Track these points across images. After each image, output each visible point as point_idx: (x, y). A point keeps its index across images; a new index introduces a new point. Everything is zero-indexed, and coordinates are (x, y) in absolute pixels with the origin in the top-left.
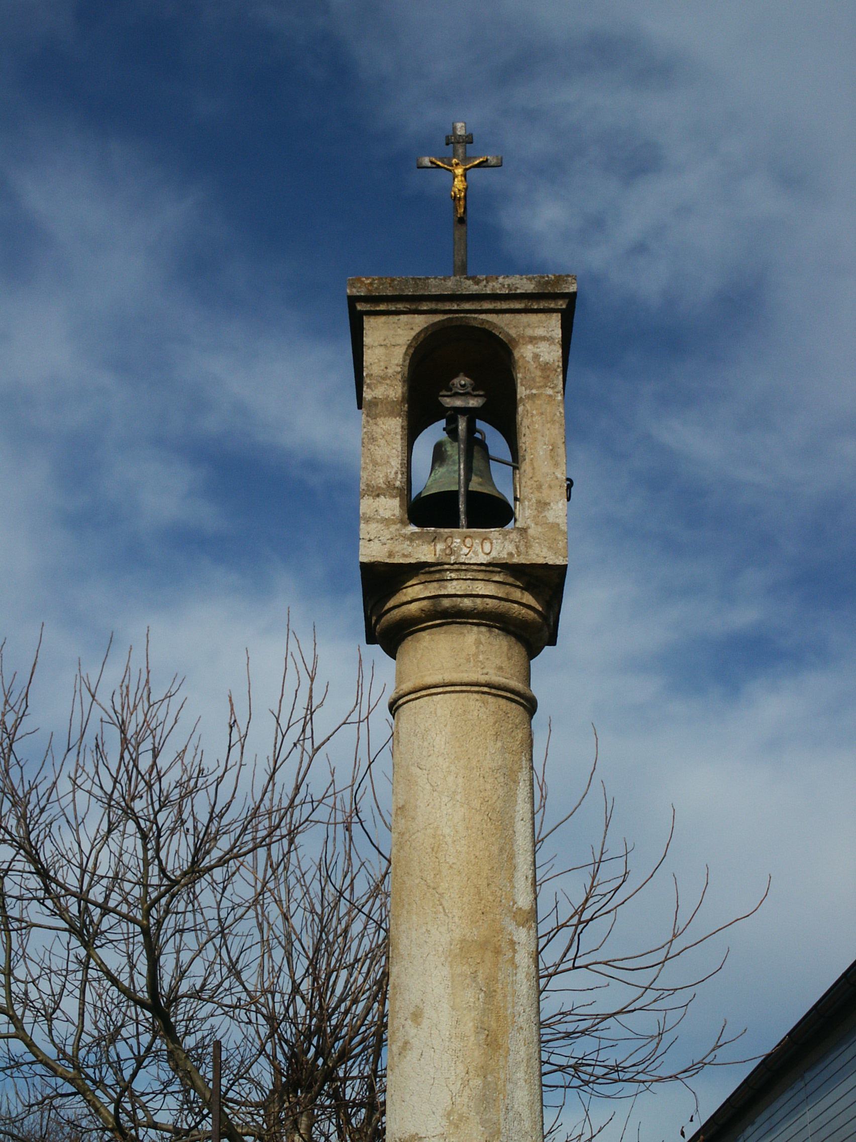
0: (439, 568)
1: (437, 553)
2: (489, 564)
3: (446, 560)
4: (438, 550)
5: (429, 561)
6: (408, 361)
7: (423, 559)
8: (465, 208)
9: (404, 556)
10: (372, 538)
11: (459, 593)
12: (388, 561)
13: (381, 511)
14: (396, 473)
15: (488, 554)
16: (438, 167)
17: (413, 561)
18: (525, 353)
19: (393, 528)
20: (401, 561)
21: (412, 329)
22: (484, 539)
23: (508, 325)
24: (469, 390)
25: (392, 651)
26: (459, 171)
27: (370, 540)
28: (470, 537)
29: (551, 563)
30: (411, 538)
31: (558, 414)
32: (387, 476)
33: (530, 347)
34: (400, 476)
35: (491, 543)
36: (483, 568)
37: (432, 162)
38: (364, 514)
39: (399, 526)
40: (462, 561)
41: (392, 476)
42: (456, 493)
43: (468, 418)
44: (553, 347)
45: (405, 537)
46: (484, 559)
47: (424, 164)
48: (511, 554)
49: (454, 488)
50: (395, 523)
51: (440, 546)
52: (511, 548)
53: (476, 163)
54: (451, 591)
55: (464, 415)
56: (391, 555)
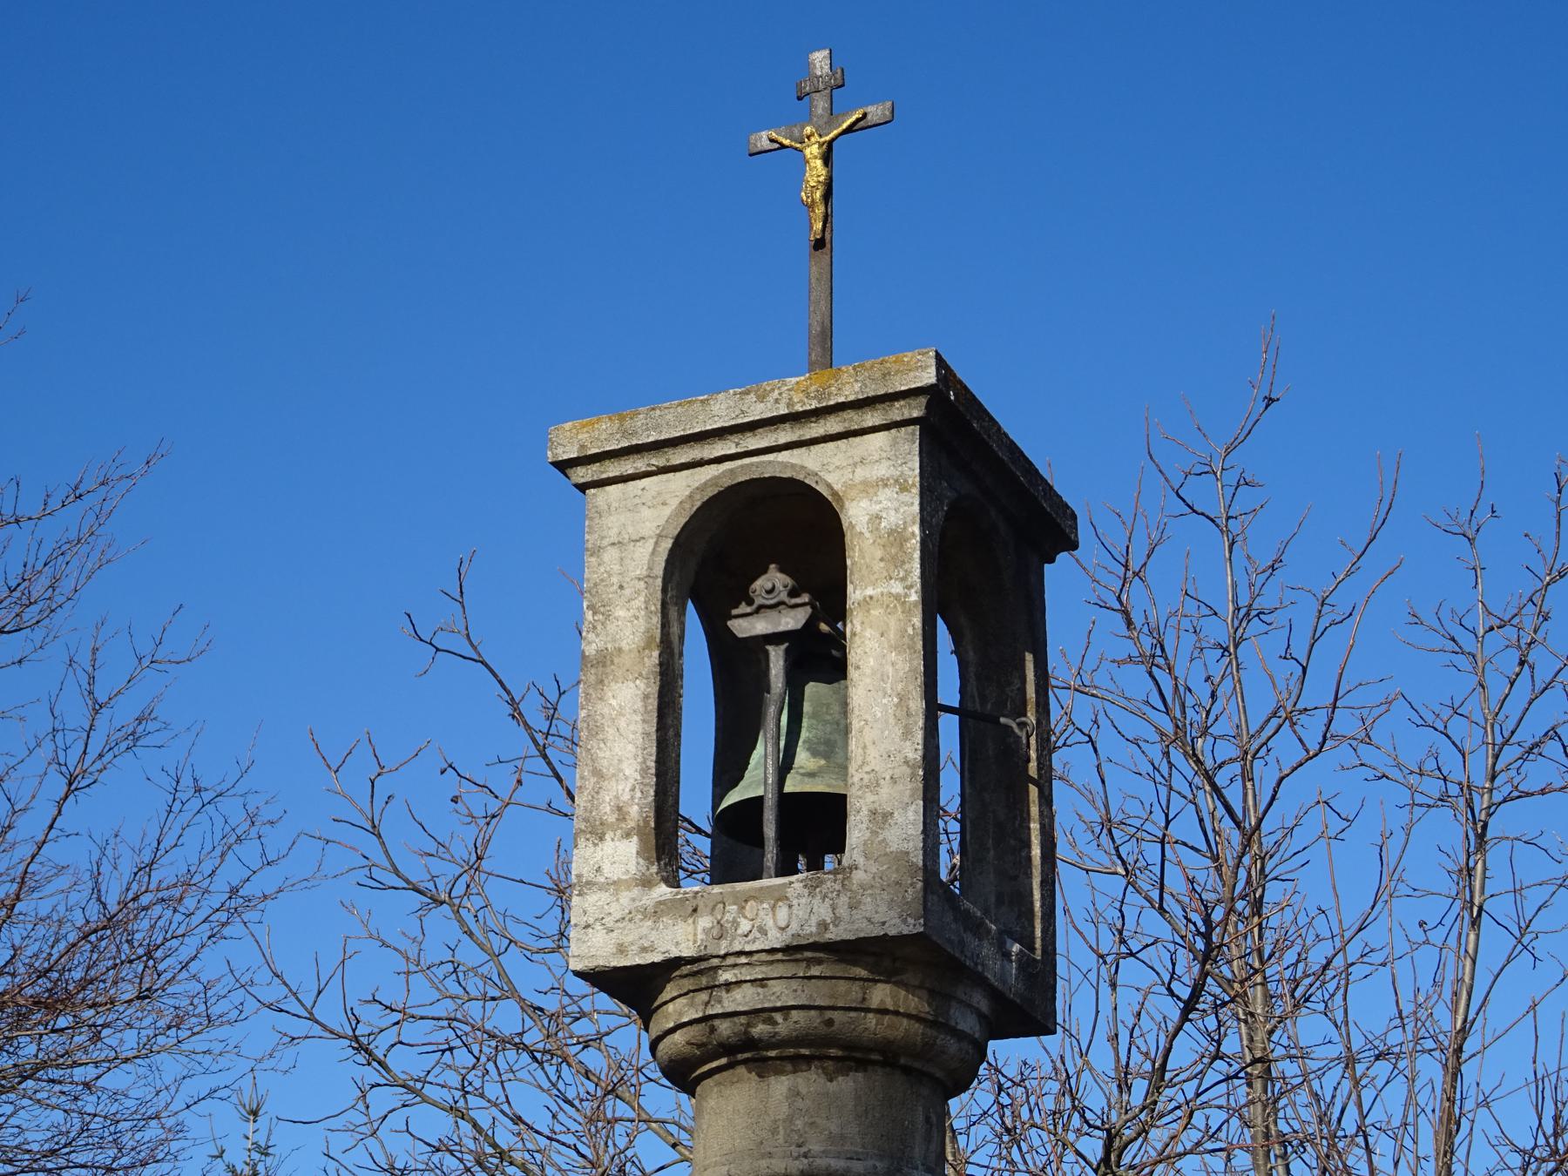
0: (703, 965)
1: (700, 937)
2: (787, 949)
3: (710, 951)
4: (700, 930)
5: (684, 955)
6: (825, 493)
7: (675, 953)
8: (826, 219)
9: (644, 950)
10: (591, 921)
11: (741, 1008)
12: (615, 963)
13: (606, 868)
14: (633, 790)
15: (783, 929)
16: (783, 146)
17: (657, 958)
18: (856, 515)
19: (625, 897)
20: (638, 961)
21: (664, 504)
22: (779, 900)
23: (823, 466)
24: (784, 596)
25: (692, 1094)
26: (813, 150)
27: (587, 926)
28: (754, 898)
29: (893, 932)
30: (657, 912)
31: (910, 631)
32: (617, 797)
33: (864, 503)
34: (638, 795)
35: (790, 907)
36: (779, 956)
37: (772, 141)
38: (579, 876)
39: (636, 891)
40: (737, 948)
41: (626, 797)
42: (759, 800)
43: (787, 651)
44: (905, 497)
45: (645, 914)
46: (775, 939)
47: (760, 148)
48: (823, 926)
49: (760, 792)
50: (628, 889)
51: (705, 922)
52: (823, 911)
53: (845, 126)
54: (729, 1007)
55: (777, 644)
56: (621, 950)
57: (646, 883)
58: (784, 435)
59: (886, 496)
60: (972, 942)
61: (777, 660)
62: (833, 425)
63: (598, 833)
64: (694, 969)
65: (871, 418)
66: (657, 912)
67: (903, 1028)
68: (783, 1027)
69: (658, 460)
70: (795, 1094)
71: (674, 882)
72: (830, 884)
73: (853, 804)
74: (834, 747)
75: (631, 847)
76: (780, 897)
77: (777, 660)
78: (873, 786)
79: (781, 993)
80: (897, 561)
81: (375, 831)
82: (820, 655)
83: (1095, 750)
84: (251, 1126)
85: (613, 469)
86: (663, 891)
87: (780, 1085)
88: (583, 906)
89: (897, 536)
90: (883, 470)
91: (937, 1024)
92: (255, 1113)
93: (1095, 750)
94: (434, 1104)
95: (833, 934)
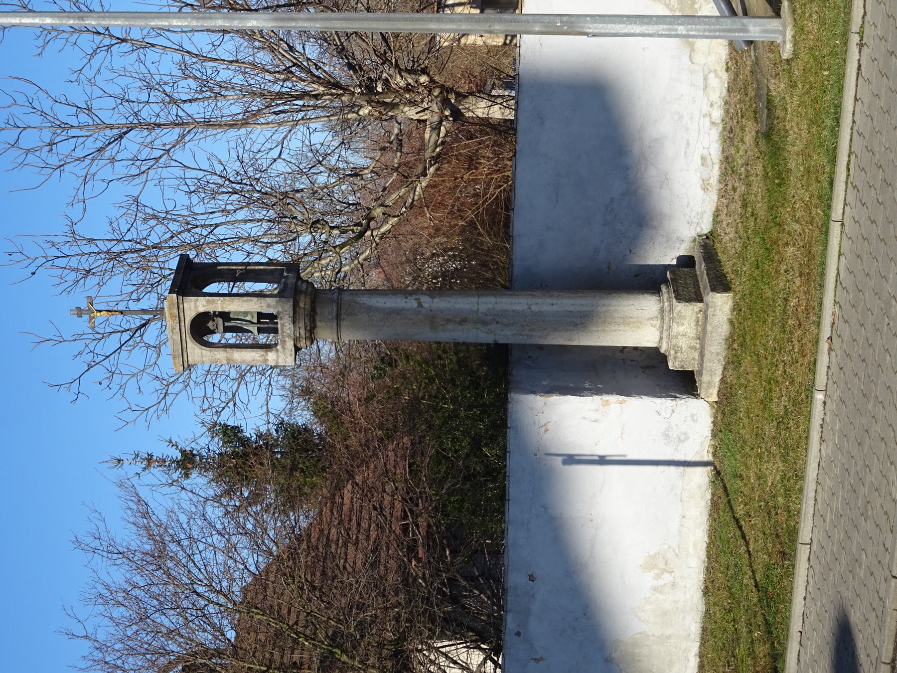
18: (202, 309)
23: (190, 315)
30: (284, 348)
46: (292, 326)
51: (287, 339)
52: (287, 317)
57: (277, 351)
58: (183, 324)
59: (198, 304)
60: (289, 286)
61: (227, 324)
62: (182, 314)
63: (266, 360)
64: (296, 340)
65: (181, 307)
66: (284, 348)
67: (308, 301)
68: (308, 324)
69: (185, 350)
70: (320, 321)
71: (276, 345)
72: (281, 315)
73: (259, 310)
74: (246, 313)
75: (269, 353)
76: (283, 325)
77: (227, 324)
78: (262, 307)
79: (302, 324)
80: (214, 302)
81: (147, 409)
82: (225, 316)
83: (602, 461)
84: (125, 462)
85: (185, 359)
86: (279, 347)
87: (318, 324)
88: (281, 363)
89: (208, 302)
90: (192, 304)
91: (306, 293)
92: (119, 461)
93: (602, 461)
94: (238, 388)
95: (292, 315)
